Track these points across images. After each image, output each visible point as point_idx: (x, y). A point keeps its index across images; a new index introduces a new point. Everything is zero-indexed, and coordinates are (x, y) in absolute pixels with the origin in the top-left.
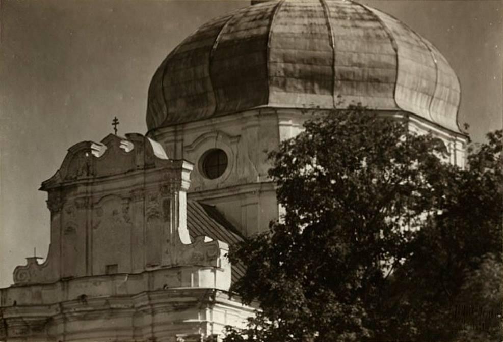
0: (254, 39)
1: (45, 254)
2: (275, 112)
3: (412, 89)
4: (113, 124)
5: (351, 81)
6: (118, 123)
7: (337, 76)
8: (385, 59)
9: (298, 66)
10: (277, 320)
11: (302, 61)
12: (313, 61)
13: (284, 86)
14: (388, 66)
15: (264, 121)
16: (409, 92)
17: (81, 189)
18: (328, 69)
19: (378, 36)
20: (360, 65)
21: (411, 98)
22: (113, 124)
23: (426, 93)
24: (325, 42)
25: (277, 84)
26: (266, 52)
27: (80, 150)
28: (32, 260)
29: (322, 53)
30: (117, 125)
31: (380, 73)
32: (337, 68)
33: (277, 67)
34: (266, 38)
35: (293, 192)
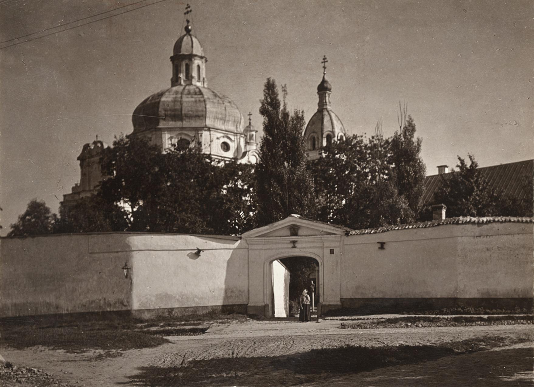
0: (155, 103)
1: (79, 182)
2: (161, 130)
3: (214, 118)
4: (322, 62)
5: (189, 117)
6: (327, 61)
7: (183, 115)
8: (200, 109)
9: (169, 112)
10: (250, 201)
11: (170, 110)
12: (175, 110)
13: (164, 119)
14: (202, 111)
15: (158, 133)
16: (213, 120)
17: (87, 160)
18: (180, 113)
19: (200, 101)
20: (192, 111)
21: (214, 122)
22: (322, 62)
23: (221, 119)
24: (179, 104)
25: (162, 119)
26: (158, 108)
27: (86, 146)
28: (76, 185)
29: (178, 107)
30: (326, 63)
31: (200, 113)
32: (183, 112)
33: (162, 112)
34: (160, 101)
35: (371, 142)
